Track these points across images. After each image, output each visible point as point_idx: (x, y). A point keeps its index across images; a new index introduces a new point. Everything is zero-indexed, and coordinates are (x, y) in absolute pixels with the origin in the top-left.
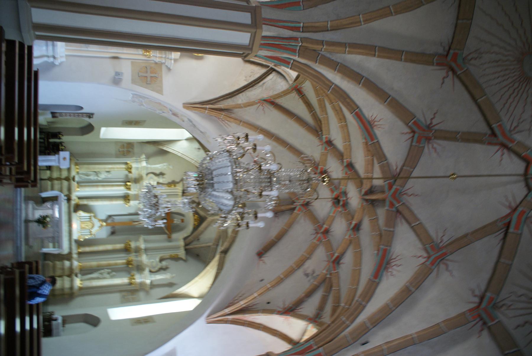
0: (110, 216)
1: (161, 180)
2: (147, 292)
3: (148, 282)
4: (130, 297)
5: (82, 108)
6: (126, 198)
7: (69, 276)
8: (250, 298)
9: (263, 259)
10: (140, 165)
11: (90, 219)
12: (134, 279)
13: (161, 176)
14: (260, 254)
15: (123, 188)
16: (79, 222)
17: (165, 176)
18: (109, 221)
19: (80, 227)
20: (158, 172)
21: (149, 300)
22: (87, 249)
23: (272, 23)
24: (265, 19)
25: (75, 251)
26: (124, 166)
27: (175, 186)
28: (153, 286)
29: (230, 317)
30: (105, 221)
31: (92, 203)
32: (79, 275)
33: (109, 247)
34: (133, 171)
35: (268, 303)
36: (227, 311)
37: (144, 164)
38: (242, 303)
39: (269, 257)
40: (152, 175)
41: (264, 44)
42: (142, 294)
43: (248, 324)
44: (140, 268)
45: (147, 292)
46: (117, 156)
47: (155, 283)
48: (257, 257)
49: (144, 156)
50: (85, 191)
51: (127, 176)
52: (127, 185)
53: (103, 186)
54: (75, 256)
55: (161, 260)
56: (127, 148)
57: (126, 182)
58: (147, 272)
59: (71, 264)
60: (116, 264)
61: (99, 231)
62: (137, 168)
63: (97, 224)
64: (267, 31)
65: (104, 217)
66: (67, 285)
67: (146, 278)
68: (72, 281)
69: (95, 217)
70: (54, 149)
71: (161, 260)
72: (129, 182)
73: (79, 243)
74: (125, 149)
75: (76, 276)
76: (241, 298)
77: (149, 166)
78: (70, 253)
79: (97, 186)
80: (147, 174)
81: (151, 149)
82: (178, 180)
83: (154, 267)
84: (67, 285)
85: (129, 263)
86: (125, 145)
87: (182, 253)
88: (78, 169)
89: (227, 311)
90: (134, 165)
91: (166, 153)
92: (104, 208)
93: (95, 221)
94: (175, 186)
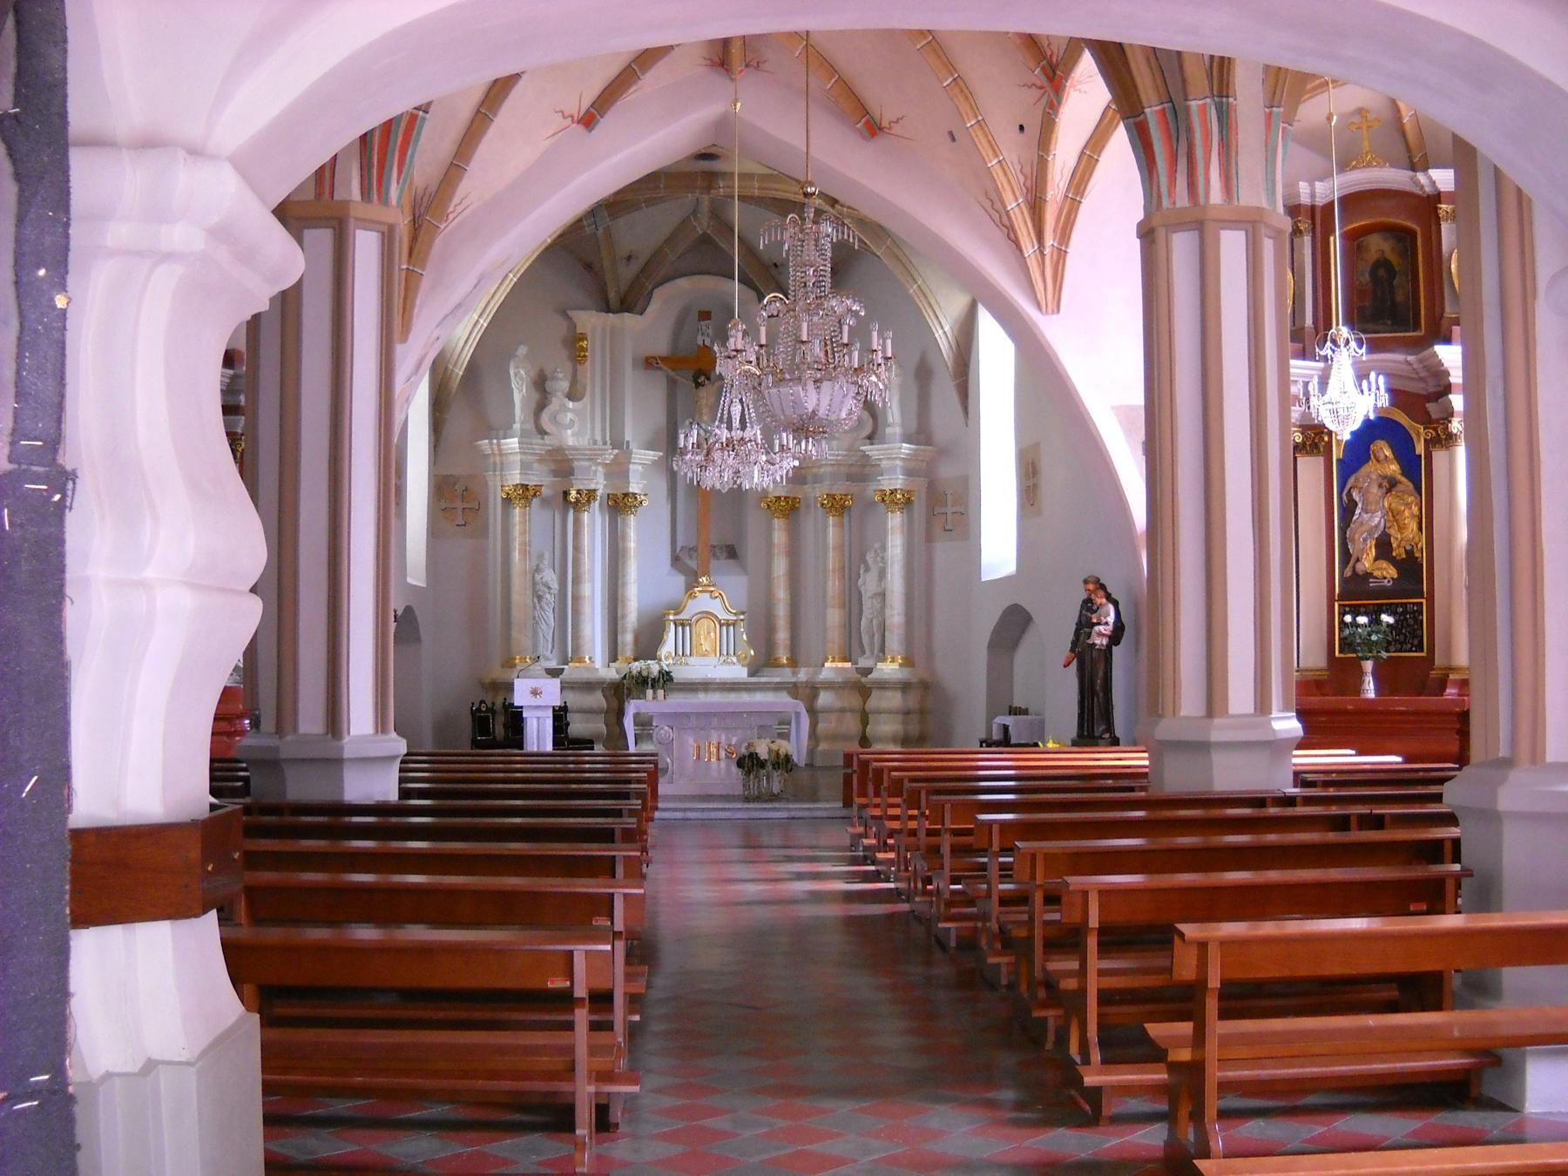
0: (676, 560)
1: (565, 385)
2: (943, 452)
3: (906, 448)
4: (950, 510)
7: (864, 691)
9: (885, 124)
11: (683, 625)
12: (893, 492)
13: (548, 385)
14: (588, 121)
16: (692, 660)
18: (693, 564)
19: (707, 654)
20: (536, 396)
21: (967, 450)
22: (782, 636)
25: (786, 675)
27: (583, 337)
28: (920, 434)
29: (1049, 241)
32: (864, 663)
33: (780, 566)
34: (532, 481)
35: (1022, 128)
36: (1029, 249)
37: (512, 443)
39: (884, 104)
42: (946, 471)
43: (1076, 194)
45: (943, 452)
46: (483, 531)
47: (913, 425)
48: (881, 141)
50: (593, 640)
51: (546, 502)
53: (577, 580)
54: (802, 675)
56: (456, 498)
57: (569, 502)
58: (872, 450)
59: (830, 686)
60: (840, 548)
62: (525, 467)
63: (704, 601)
65: (680, 580)
66: (894, 700)
67: (894, 458)
68: (883, 685)
70: (497, 723)
72: (566, 494)
73: (763, 661)
74: (459, 505)
75: (869, 671)
76: (998, 205)
77: (517, 426)
78: (793, 689)
79: (577, 598)
80: (542, 432)
81: (458, 421)
84: (894, 700)
85: (837, 506)
88: (523, 659)
89: (1029, 249)
90: (515, 477)
91: (473, 368)
92: (648, 578)
93: (691, 609)
94: (583, 337)
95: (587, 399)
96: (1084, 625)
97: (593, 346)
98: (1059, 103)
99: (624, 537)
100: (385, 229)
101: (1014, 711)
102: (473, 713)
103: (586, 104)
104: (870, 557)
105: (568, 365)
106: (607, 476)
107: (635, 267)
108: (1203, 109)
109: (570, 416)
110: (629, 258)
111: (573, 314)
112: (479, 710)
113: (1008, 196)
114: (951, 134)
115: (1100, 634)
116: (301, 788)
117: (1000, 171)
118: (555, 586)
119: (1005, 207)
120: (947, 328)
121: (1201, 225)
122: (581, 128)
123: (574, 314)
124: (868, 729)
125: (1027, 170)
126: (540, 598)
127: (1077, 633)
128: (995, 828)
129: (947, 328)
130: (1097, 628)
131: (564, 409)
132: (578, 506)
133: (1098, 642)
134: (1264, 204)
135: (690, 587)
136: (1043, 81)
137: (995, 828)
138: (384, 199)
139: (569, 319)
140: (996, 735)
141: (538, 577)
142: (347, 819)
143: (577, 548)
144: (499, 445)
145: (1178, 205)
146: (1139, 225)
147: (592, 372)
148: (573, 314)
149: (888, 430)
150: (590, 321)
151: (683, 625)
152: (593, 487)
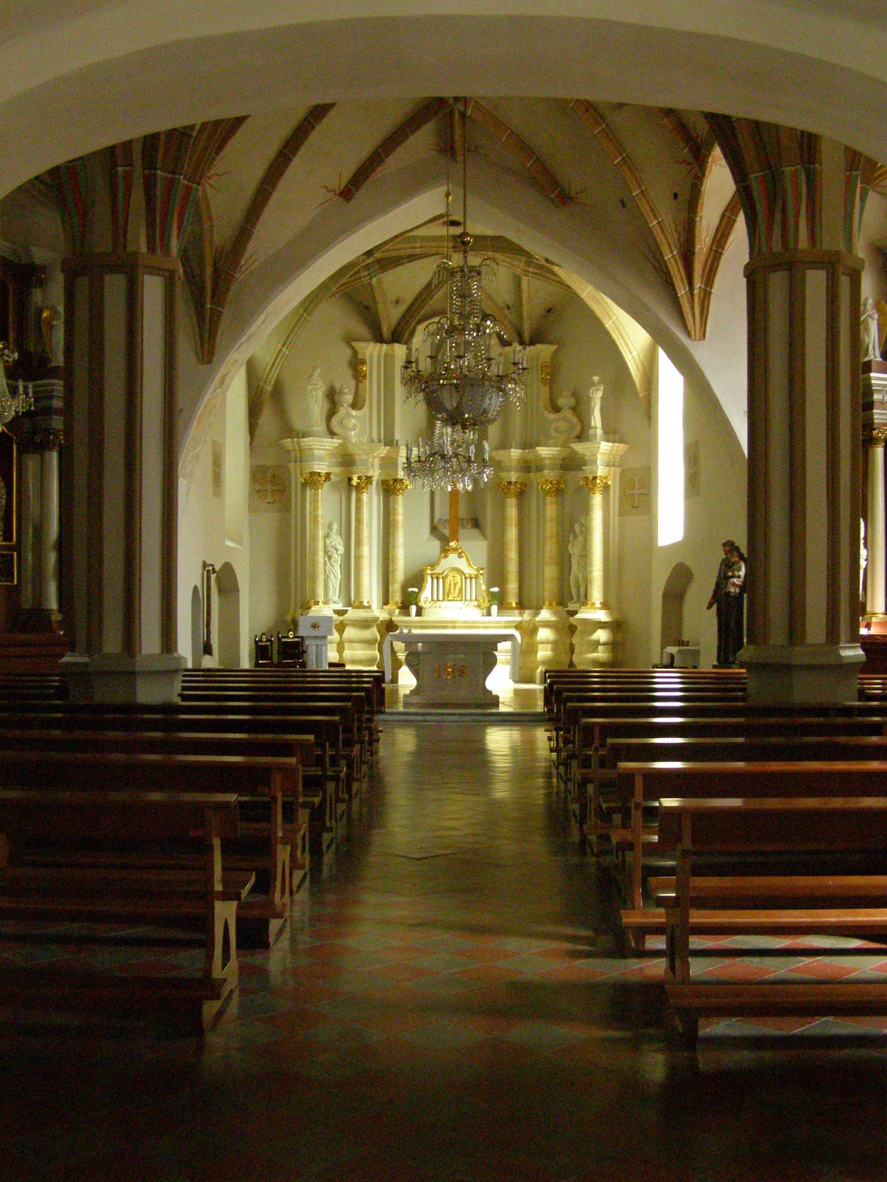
0: (434, 529)
1: (349, 398)
5: (196, 588)
6: (389, 489)
8: (660, 238)
9: (573, 194)
10: (321, 452)
13: (336, 397)
14: (347, 194)
15: (365, 497)
17: (337, 387)
18: (447, 532)
20: (326, 406)
23: (120, 232)
24: (115, 246)
26: (309, 493)
27: (363, 362)
29: (698, 284)
30: (445, 541)
31: (399, 576)
32: (571, 606)
35: (676, 196)
38: (668, 257)
40: (334, 421)
41: (162, 246)
43: (719, 246)
44: (571, 464)
46: (285, 508)
49: (288, 443)
51: (335, 486)
52: (359, 484)
53: (358, 544)
55: (556, 409)
57: (350, 487)
61: (465, 561)
63: (453, 560)
64: (139, 241)
65: (436, 544)
69: (433, 566)
71: (556, 409)
72: (350, 479)
74: (269, 487)
75: (573, 613)
81: (267, 418)
82: (349, 352)
83: (572, 427)
85: (559, 491)
86: (257, 487)
87: (544, 351)
89: (682, 291)
94: (363, 362)
95: (366, 408)
96: (723, 579)
97: (372, 370)
98: (704, 175)
99: (395, 512)
100: (167, 274)
101: (681, 643)
102: (256, 642)
103: (344, 182)
104: (577, 527)
105: (353, 383)
106: (382, 467)
107: (402, 308)
108: (795, 175)
109: (353, 421)
110: (397, 302)
111: (354, 344)
112: (260, 640)
113: (665, 249)
114: (622, 201)
115: (734, 584)
116: (106, 693)
117: (658, 230)
118: (341, 549)
119: (663, 258)
120: (635, 354)
121: (792, 266)
122: (341, 200)
123: (358, 345)
124: (574, 656)
125: (680, 229)
126: (330, 557)
127: (718, 585)
128: (597, 729)
129: (635, 354)
130: (731, 580)
131: (349, 416)
132: (358, 488)
133: (732, 590)
134: (842, 247)
135: (445, 551)
136: (691, 158)
137: (597, 729)
138: (166, 249)
139: (353, 348)
140: (666, 661)
141: (328, 542)
142: (139, 716)
143: (359, 521)
144: (298, 443)
145: (774, 250)
146: (747, 267)
147: (372, 387)
148: (354, 344)
149: (591, 432)
150: (372, 351)
151: (438, 578)
152: (370, 474)
